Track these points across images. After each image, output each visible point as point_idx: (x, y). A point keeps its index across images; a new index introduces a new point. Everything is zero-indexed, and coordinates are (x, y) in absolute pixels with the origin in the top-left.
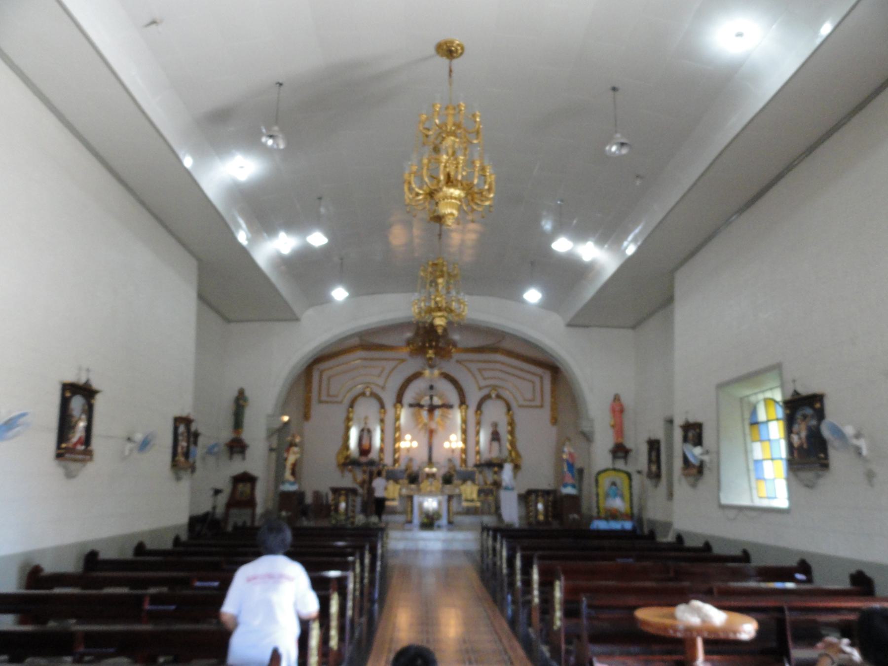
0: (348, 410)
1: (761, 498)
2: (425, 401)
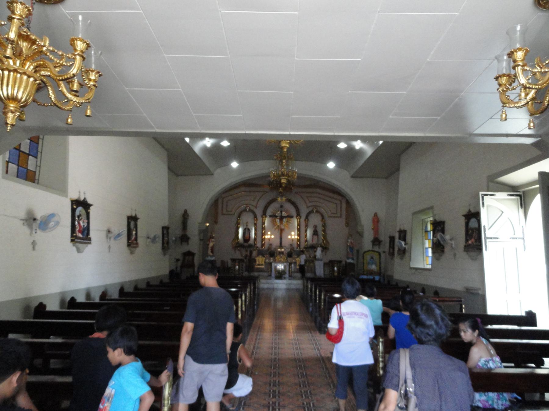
0: (237, 219)
1: (427, 264)
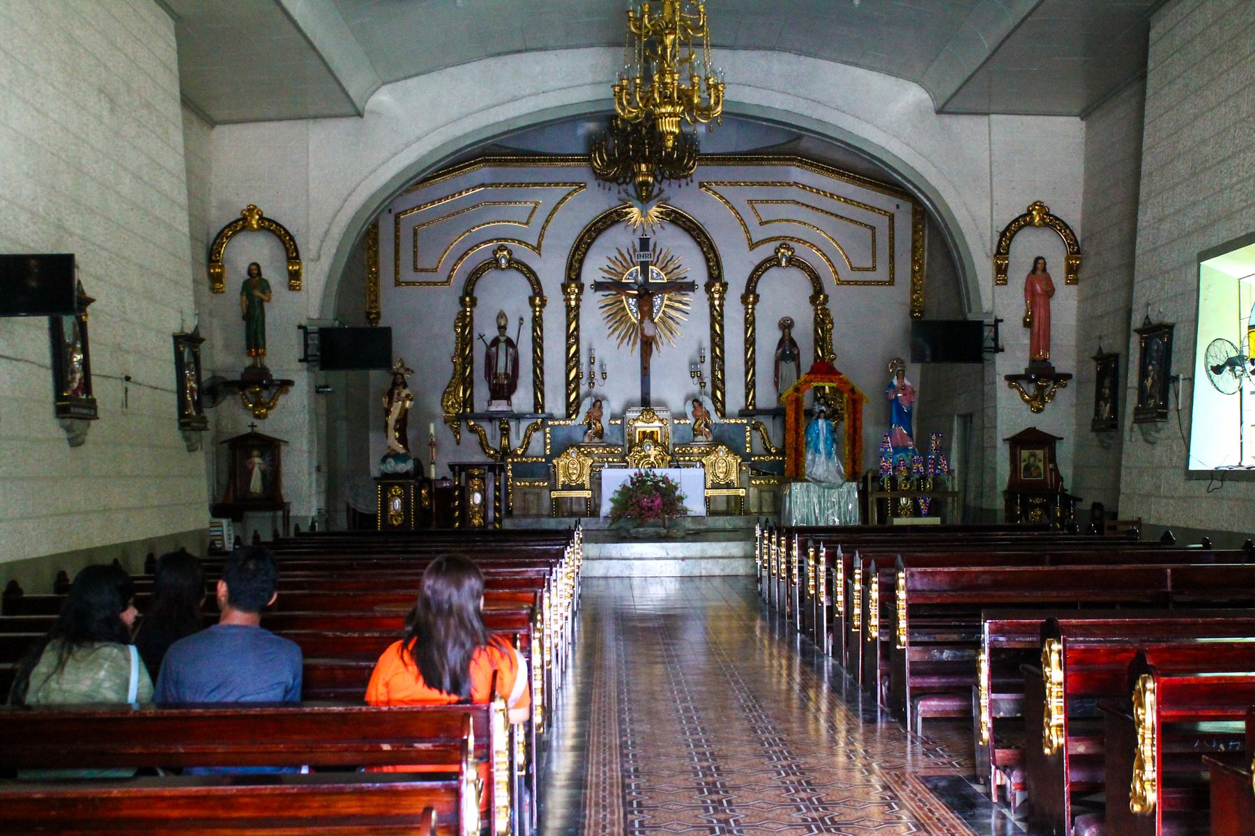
0: (462, 301)
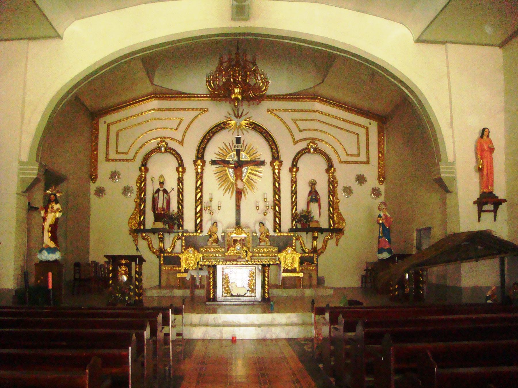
2: (232, 157)
